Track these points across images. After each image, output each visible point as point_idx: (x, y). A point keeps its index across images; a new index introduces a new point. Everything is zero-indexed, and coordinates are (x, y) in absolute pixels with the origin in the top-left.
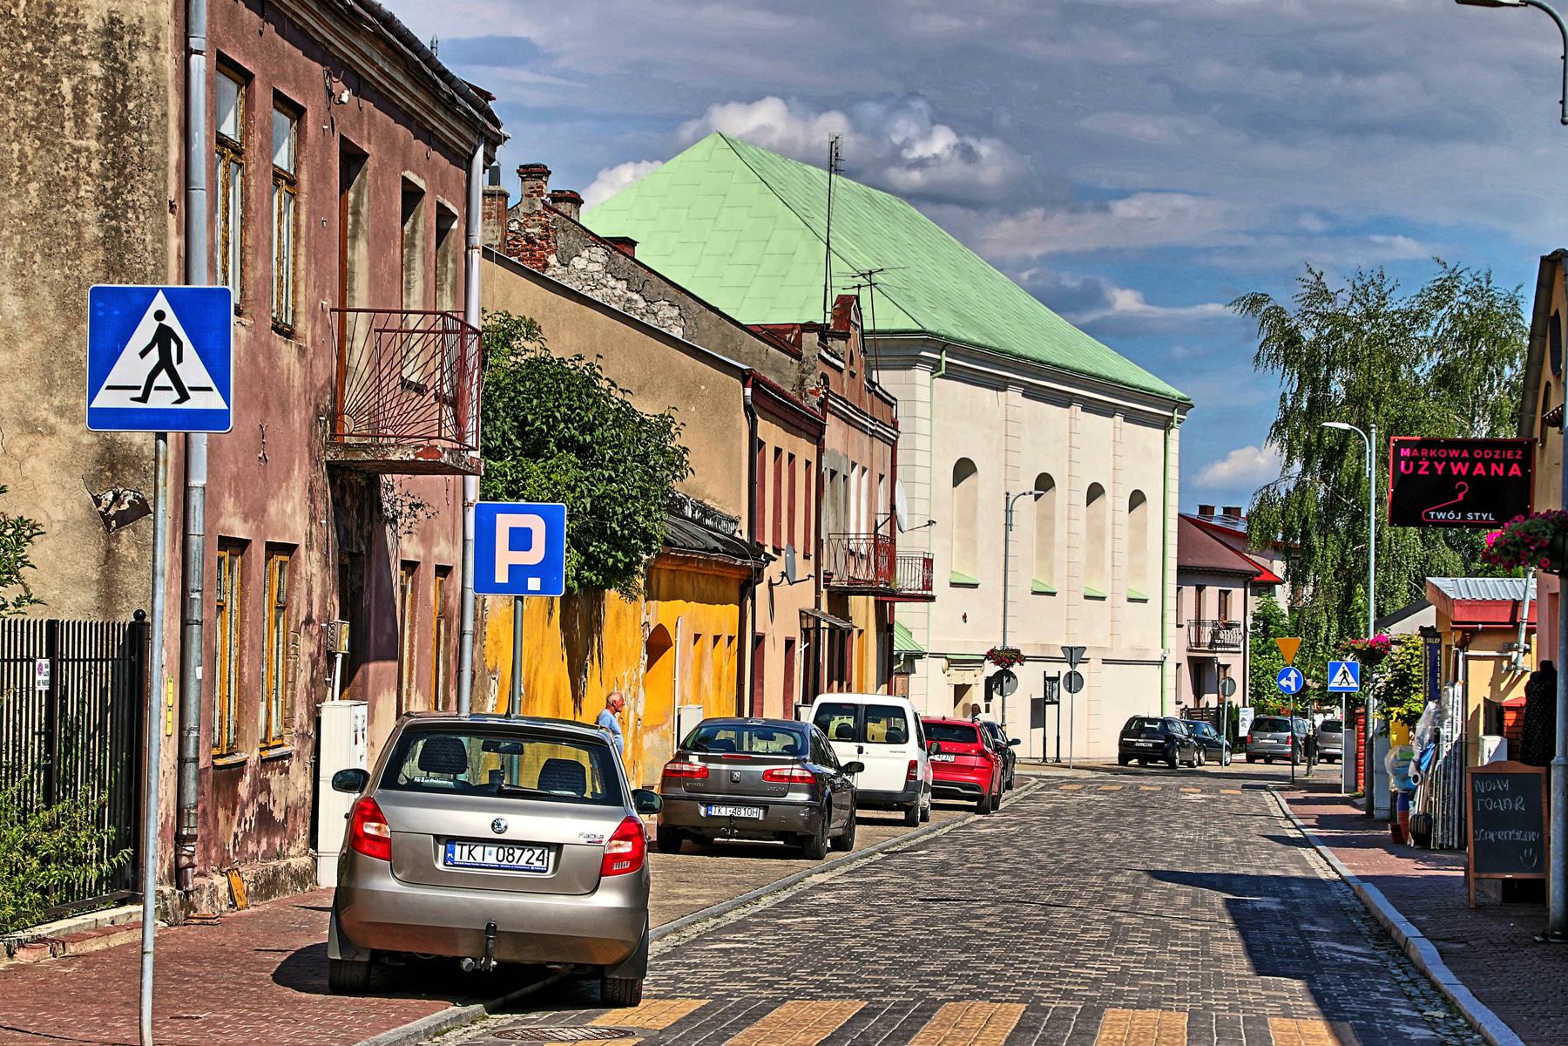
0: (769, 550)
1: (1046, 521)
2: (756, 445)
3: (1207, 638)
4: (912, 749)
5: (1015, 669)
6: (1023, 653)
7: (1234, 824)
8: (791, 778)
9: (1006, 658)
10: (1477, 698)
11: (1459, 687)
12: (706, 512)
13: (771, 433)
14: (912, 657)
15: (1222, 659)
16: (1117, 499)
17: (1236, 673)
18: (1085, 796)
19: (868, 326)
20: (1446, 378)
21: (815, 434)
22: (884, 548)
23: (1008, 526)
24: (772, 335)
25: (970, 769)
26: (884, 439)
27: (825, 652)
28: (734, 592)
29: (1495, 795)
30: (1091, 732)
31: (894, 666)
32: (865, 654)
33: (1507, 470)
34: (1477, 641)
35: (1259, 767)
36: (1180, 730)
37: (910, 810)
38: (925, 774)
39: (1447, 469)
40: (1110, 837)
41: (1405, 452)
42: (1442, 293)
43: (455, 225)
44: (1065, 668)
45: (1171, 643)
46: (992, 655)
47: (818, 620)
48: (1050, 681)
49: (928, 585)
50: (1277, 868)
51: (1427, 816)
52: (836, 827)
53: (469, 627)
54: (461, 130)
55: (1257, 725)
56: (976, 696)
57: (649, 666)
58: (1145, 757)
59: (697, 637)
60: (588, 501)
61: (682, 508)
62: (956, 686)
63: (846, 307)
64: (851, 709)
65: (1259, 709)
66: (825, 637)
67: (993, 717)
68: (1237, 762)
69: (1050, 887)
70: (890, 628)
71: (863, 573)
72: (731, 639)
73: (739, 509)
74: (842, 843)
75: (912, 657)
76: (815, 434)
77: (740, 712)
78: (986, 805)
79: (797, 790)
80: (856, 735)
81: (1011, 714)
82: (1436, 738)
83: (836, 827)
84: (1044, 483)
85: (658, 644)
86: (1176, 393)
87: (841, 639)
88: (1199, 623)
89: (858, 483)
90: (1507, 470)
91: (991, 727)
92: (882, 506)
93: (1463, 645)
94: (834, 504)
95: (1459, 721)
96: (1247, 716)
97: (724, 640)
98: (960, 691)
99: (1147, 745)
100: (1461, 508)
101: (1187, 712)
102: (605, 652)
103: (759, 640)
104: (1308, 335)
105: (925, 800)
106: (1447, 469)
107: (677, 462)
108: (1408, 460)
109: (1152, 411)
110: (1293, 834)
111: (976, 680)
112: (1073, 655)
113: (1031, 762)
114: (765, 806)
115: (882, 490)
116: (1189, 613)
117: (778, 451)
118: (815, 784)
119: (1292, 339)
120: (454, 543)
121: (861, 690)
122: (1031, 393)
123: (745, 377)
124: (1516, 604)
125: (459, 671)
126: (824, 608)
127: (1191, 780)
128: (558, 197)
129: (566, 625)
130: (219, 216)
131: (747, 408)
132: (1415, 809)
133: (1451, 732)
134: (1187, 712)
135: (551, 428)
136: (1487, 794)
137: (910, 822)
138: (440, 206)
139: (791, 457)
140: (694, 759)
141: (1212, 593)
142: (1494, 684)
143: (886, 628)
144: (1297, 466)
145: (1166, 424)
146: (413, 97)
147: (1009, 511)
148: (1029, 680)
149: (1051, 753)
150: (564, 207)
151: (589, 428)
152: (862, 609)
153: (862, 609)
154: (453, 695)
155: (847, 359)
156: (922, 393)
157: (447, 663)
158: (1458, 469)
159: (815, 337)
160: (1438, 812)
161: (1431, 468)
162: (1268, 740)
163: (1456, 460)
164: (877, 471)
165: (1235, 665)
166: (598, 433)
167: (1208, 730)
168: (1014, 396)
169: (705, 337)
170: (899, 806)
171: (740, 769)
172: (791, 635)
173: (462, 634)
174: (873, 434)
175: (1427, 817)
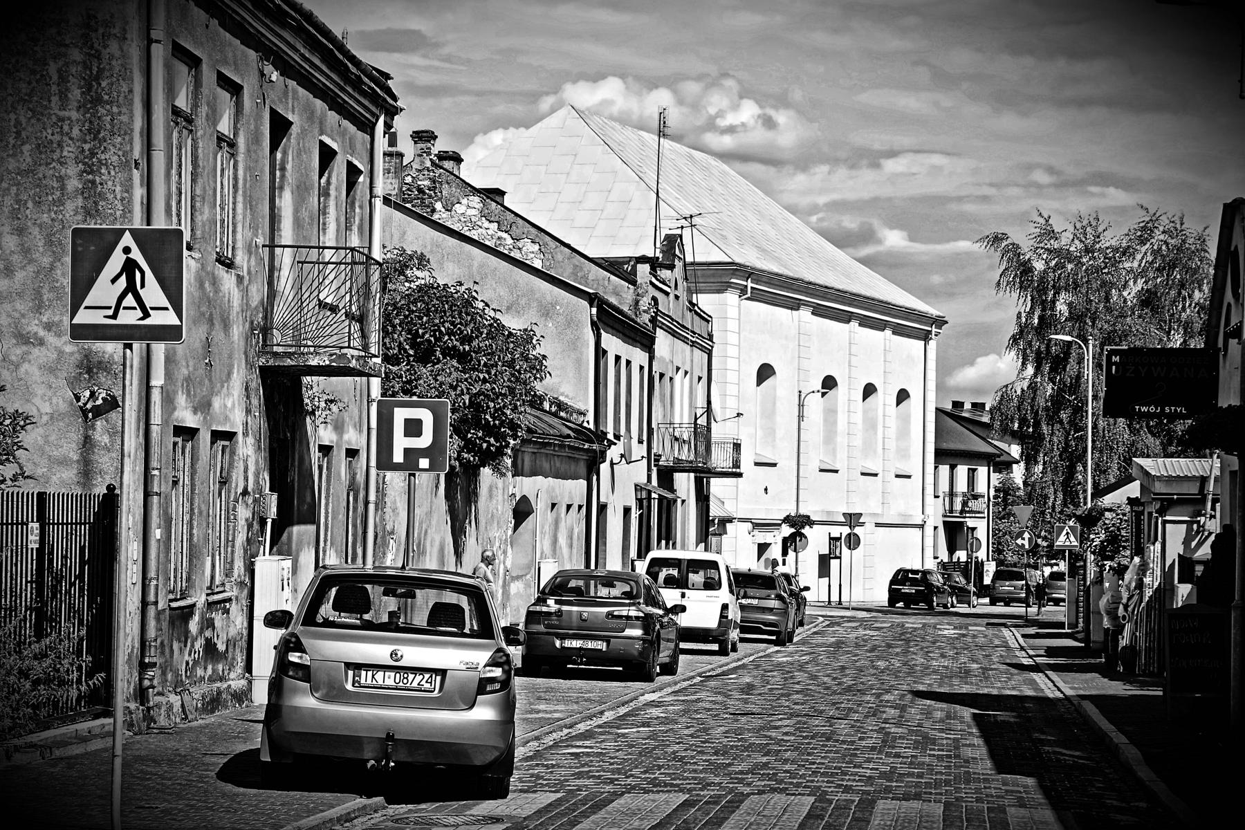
0: (610, 436)
2: (600, 353)
3: (958, 506)
4: (724, 595)
5: (806, 531)
6: (586, 312)
8: (628, 618)
9: (799, 522)
10: (1175, 548)
11: (1158, 545)
12: (561, 406)
13: (612, 344)
14: (724, 521)
15: (971, 523)
16: (886, 396)
17: (981, 534)
18: (861, 632)
19: (689, 259)
20: (1148, 300)
21: (647, 343)
22: (702, 435)
23: (801, 417)
24: (613, 266)
25: (771, 610)
26: (702, 349)
27: (655, 517)
28: (582, 469)
31: (710, 528)
32: (687, 519)
35: (1000, 609)
36: (937, 580)
38: (734, 614)
40: (881, 664)
41: (1116, 359)
43: (361, 179)
44: (846, 530)
45: (929, 510)
46: (788, 520)
47: (649, 492)
48: (834, 540)
49: (737, 464)
52: (664, 656)
53: (372, 497)
54: (366, 103)
55: (998, 576)
56: (775, 552)
57: (516, 528)
58: (909, 600)
59: (553, 505)
60: (467, 398)
61: (541, 403)
62: (759, 545)
63: (672, 243)
64: (676, 563)
65: (1000, 563)
67: (789, 569)
68: (982, 605)
69: (834, 704)
70: (707, 498)
71: (685, 454)
72: (580, 507)
73: (586, 403)
74: (669, 669)
75: (724, 521)
76: (647, 343)
78: (783, 639)
79: (633, 627)
80: (680, 583)
82: (1140, 585)
83: (664, 656)
84: (829, 383)
85: (522, 511)
86: (933, 311)
87: (667, 507)
88: (952, 494)
89: (681, 384)
91: (787, 577)
92: (701, 402)
93: (1162, 512)
94: (662, 400)
95: (1158, 572)
96: (990, 568)
98: (763, 548)
99: (910, 590)
101: (943, 565)
104: (1039, 266)
105: (734, 634)
107: (538, 366)
109: (917, 326)
111: (775, 539)
112: (853, 519)
114: (607, 640)
115: (701, 389)
116: (944, 487)
117: (618, 358)
118: (647, 622)
119: (1026, 268)
121: (683, 547)
122: (818, 311)
123: (592, 299)
124: (1203, 480)
127: (946, 619)
128: (443, 156)
130: (174, 172)
131: (593, 323)
133: (1152, 581)
134: (943, 565)
137: (723, 652)
138: (350, 164)
139: (628, 362)
140: (551, 602)
142: (1186, 542)
143: (703, 498)
144: (1030, 370)
145: (926, 337)
146: (328, 77)
147: (801, 405)
148: (817, 539)
149: (835, 598)
150: (448, 165)
151: (467, 339)
152: (684, 483)
153: (684, 483)
154: (360, 551)
155: (673, 285)
156: (732, 312)
157: (355, 526)
159: (647, 267)
162: (1006, 587)
165: (981, 527)
166: (475, 343)
167: (959, 579)
168: (805, 314)
171: (587, 610)
172: (628, 504)
173: (367, 503)
174: (693, 344)
175: (1132, 649)
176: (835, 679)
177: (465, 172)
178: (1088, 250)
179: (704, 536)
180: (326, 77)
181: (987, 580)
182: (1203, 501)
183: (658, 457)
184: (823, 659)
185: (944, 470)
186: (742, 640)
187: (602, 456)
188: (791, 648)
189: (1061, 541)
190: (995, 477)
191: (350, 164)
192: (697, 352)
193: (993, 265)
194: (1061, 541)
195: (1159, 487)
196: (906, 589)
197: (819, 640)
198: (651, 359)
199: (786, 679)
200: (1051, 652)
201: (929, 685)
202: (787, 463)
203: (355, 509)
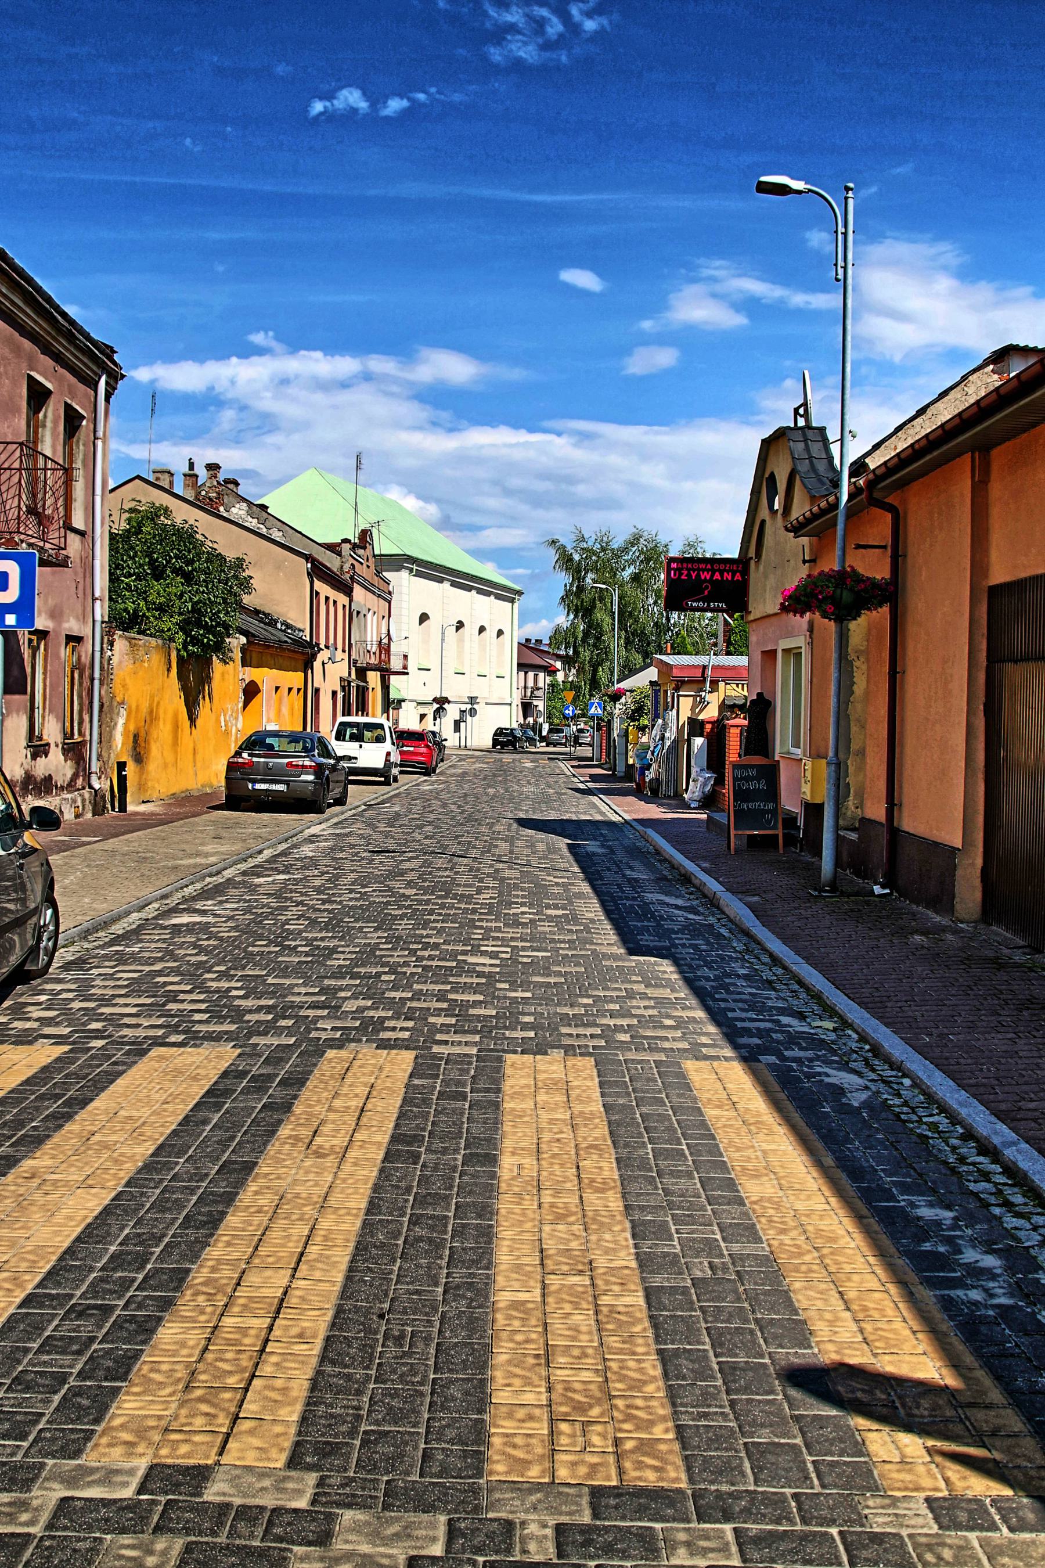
0: (322, 646)
1: (461, 641)
3: (529, 694)
4: (387, 746)
5: (446, 706)
6: (305, 566)
7: (551, 780)
8: (303, 766)
9: (441, 702)
10: (685, 714)
11: (675, 711)
12: (288, 626)
13: (323, 589)
14: (400, 702)
15: (535, 703)
16: (491, 632)
17: (541, 708)
18: (478, 765)
19: (377, 552)
20: (636, 578)
21: (348, 592)
22: (385, 648)
23: (443, 640)
25: (421, 754)
26: (385, 599)
27: (354, 697)
28: (301, 665)
29: (747, 779)
30: (480, 733)
31: (390, 704)
32: (375, 698)
33: (733, 576)
34: (685, 687)
35: (551, 749)
36: (518, 733)
37: (387, 777)
38: (395, 758)
39: (698, 575)
40: (491, 791)
41: (674, 565)
42: (634, 541)
43: (84, 423)
44: (469, 706)
45: (514, 695)
46: (435, 700)
47: (349, 683)
48: (462, 712)
49: (405, 667)
50: (585, 813)
51: (657, 780)
52: (336, 791)
53: (97, 675)
54: (86, 360)
55: (550, 731)
56: (430, 717)
57: (246, 704)
58: (503, 745)
59: (277, 688)
60: (190, 605)
63: (365, 536)
64: (356, 725)
65: (551, 724)
66: (354, 692)
67: (436, 729)
68: (542, 747)
69: (457, 837)
70: (388, 687)
71: (373, 661)
72: (299, 690)
73: (304, 623)
74: (341, 801)
75: (400, 702)
76: (348, 592)
77: (305, 728)
78: (428, 771)
79: (308, 773)
80: (358, 738)
81: (445, 728)
82: (662, 738)
83: (336, 791)
84: (460, 625)
85: (251, 691)
86: (517, 588)
87: (362, 692)
88: (525, 687)
89: (371, 620)
90: (733, 576)
91: (434, 733)
92: (384, 630)
93: (677, 689)
94: (359, 627)
95: (674, 729)
96: (546, 727)
97: (295, 691)
98: (423, 716)
99: (504, 740)
100: (708, 599)
101: (521, 725)
102: (215, 693)
103: (317, 690)
104: (577, 557)
105: (395, 771)
106: (698, 575)
107: (245, 584)
108: (675, 570)
109: (507, 595)
110: (581, 786)
111: (430, 711)
112: (472, 700)
113: (453, 748)
114: (287, 783)
115: (384, 622)
117: (327, 598)
118: (319, 770)
119: (570, 559)
120: (84, 622)
121: (373, 716)
122: (454, 584)
123: (308, 558)
124: (705, 667)
125: (91, 703)
126: (353, 676)
127: (525, 756)
128: (227, 481)
129: (180, 677)
131: (309, 574)
132: (650, 775)
133: (671, 735)
134: (521, 725)
135: (168, 562)
136: (742, 779)
137: (387, 783)
138: (68, 407)
139: (335, 602)
140: (245, 755)
141: (531, 675)
142: (693, 709)
143: (386, 687)
144: (572, 616)
145: (512, 601)
146: (35, 322)
148: (452, 712)
149: (463, 744)
150: (231, 486)
151: (190, 562)
152: (374, 679)
153: (374, 679)
154: (86, 718)
156: (405, 583)
157: (80, 697)
158: (705, 575)
160: (663, 777)
161: (689, 575)
162: (555, 737)
163: (703, 570)
164: (381, 614)
165: (540, 705)
166: (196, 565)
167: (531, 733)
168: (446, 585)
169: (290, 542)
170: (383, 776)
171: (272, 761)
173: (92, 679)
174: (379, 596)
175: (656, 781)
176: (459, 806)
177: (241, 491)
178: (603, 549)
179: (386, 710)
180: (29, 317)
181: (544, 733)
182: (704, 681)
183: (355, 662)
184: (453, 787)
185: (522, 674)
186: (401, 772)
187: (314, 657)
188: (434, 778)
189: (592, 711)
190: (548, 679)
191: (68, 407)
192: (382, 601)
193: (552, 555)
194: (592, 711)
195: (675, 672)
196: (501, 739)
197: (452, 771)
198: (351, 601)
199: (424, 807)
200: (594, 778)
201: (527, 811)
202: (435, 666)
203: (81, 684)
